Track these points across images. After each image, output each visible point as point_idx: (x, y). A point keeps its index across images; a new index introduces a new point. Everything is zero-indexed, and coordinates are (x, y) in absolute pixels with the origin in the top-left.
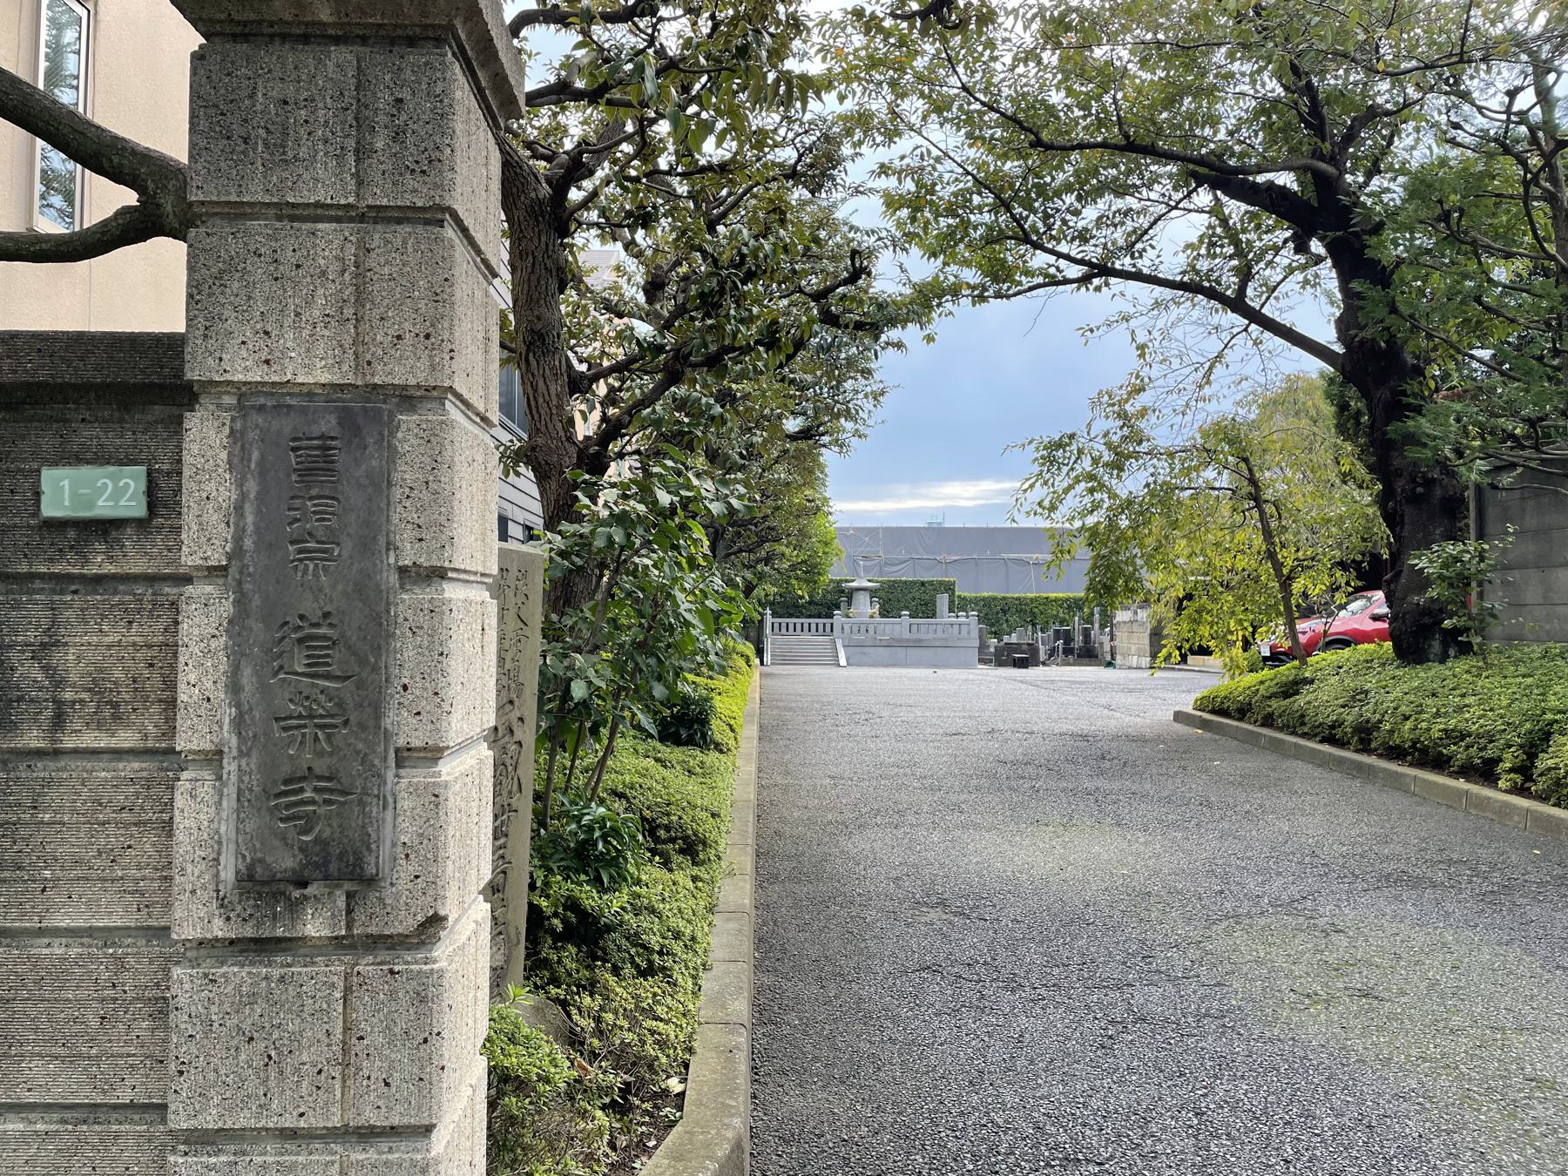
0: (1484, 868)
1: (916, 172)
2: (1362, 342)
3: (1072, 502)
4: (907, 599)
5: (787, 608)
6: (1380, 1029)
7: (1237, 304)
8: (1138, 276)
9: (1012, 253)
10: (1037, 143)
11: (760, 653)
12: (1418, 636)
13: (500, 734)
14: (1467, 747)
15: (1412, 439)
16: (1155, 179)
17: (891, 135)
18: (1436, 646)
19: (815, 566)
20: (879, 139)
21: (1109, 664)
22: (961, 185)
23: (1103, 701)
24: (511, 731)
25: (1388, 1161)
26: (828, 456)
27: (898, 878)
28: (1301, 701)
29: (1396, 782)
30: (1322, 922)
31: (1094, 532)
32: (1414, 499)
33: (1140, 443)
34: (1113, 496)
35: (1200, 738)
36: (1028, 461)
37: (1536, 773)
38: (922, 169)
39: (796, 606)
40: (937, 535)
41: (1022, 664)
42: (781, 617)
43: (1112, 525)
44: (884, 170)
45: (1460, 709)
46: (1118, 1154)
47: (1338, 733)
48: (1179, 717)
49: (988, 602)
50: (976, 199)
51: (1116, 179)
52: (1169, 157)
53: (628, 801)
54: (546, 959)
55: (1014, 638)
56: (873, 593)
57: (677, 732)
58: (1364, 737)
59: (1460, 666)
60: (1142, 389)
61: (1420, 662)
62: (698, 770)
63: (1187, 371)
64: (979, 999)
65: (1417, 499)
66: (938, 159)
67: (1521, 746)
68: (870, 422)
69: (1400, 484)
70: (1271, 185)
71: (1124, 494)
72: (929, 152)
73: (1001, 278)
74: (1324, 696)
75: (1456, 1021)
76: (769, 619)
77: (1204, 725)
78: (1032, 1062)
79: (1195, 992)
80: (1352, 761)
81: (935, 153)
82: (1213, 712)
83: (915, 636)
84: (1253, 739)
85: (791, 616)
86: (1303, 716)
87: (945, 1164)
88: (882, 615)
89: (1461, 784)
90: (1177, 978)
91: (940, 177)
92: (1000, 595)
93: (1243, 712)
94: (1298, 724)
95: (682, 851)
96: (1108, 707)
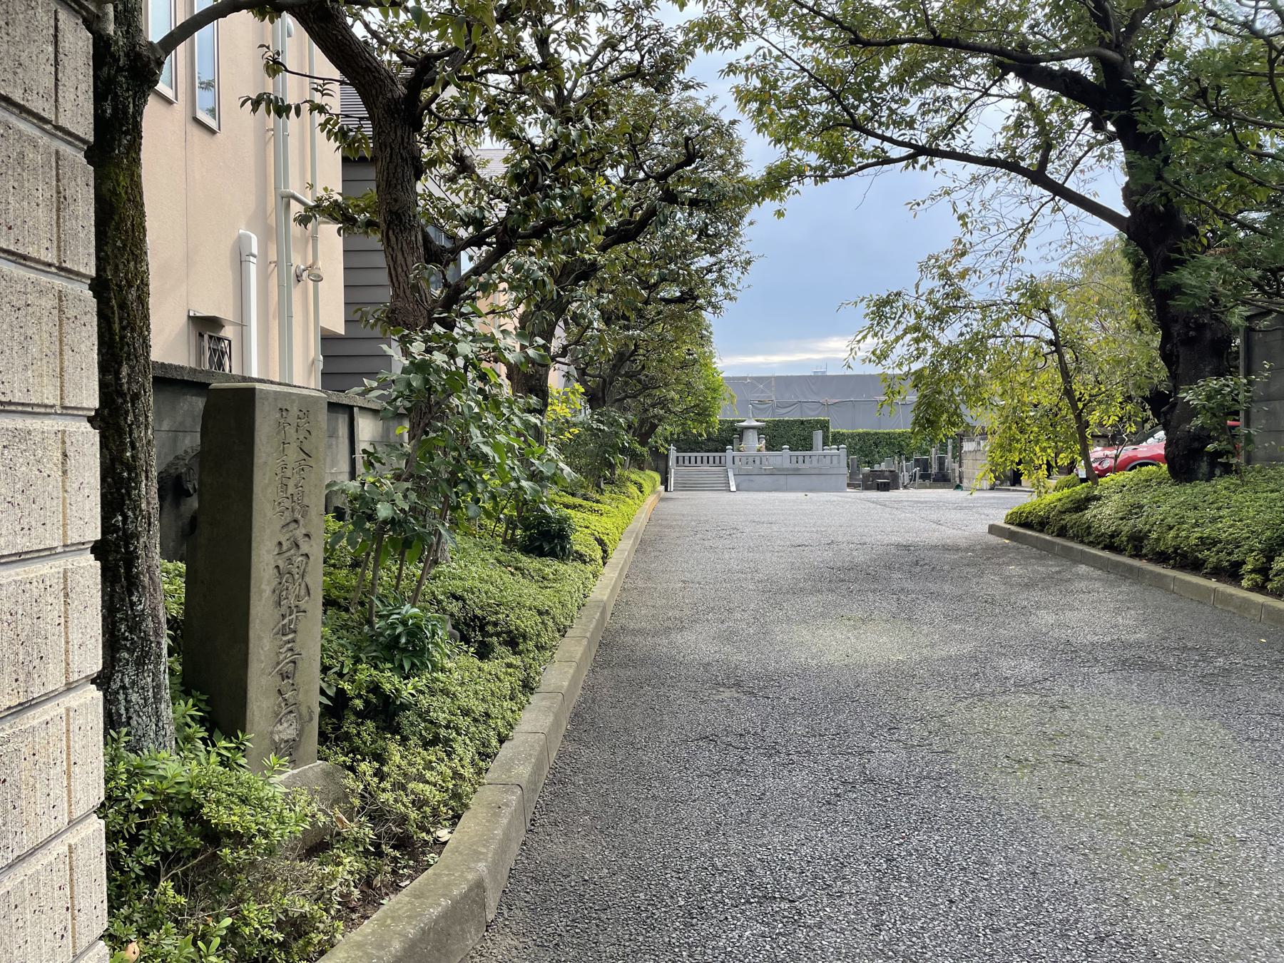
0: (1211, 654)
1: (760, 71)
2: (1144, 207)
3: (900, 350)
4: (789, 435)
5: (689, 444)
6: (1071, 790)
7: (1038, 176)
8: (952, 155)
9: (851, 137)
10: (856, 41)
11: (665, 482)
12: (1187, 461)
13: (285, 548)
14: (1218, 552)
15: (1177, 289)
16: (972, 71)
17: (737, 39)
18: (1204, 467)
19: (706, 409)
20: (727, 42)
21: (958, 487)
22: (799, 80)
23: (934, 517)
24: (297, 546)
25: (1040, 903)
26: (707, 315)
27: (709, 664)
28: (1088, 514)
29: (1159, 582)
30: (1052, 700)
31: (919, 375)
32: (1188, 342)
33: (958, 299)
34: (937, 344)
35: (1005, 547)
36: (860, 316)
37: (1271, 573)
38: (765, 67)
39: (697, 442)
40: (819, 382)
41: (884, 487)
42: (685, 451)
43: (935, 368)
44: (732, 69)
45: (1214, 520)
46: (810, 893)
47: (1117, 541)
48: (993, 529)
49: (863, 437)
50: (813, 92)
51: (938, 70)
52: (977, 50)
53: (464, 600)
54: (347, 733)
55: (883, 466)
56: (760, 430)
57: (541, 545)
58: (1137, 544)
59: (1221, 483)
60: (963, 254)
61: (1190, 482)
62: (551, 576)
63: (1003, 236)
64: (739, 764)
65: (1191, 339)
66: (778, 59)
67: (1262, 551)
68: (738, 287)
69: (1176, 329)
70: (1065, 73)
71: (945, 343)
72: (770, 52)
73: (838, 162)
74: (1105, 514)
75: (1141, 784)
76: (673, 454)
77: (1012, 536)
78: (764, 816)
79: (923, 758)
80: (1125, 565)
81: (775, 53)
82: (1020, 525)
83: (795, 466)
84: (1048, 548)
85: (692, 451)
86: (1089, 527)
87: (663, 900)
88: (768, 449)
89: (1213, 583)
90: (913, 746)
91: (781, 73)
92: (873, 431)
93: (1042, 525)
94: (1085, 534)
95: (506, 643)
96: (938, 523)
